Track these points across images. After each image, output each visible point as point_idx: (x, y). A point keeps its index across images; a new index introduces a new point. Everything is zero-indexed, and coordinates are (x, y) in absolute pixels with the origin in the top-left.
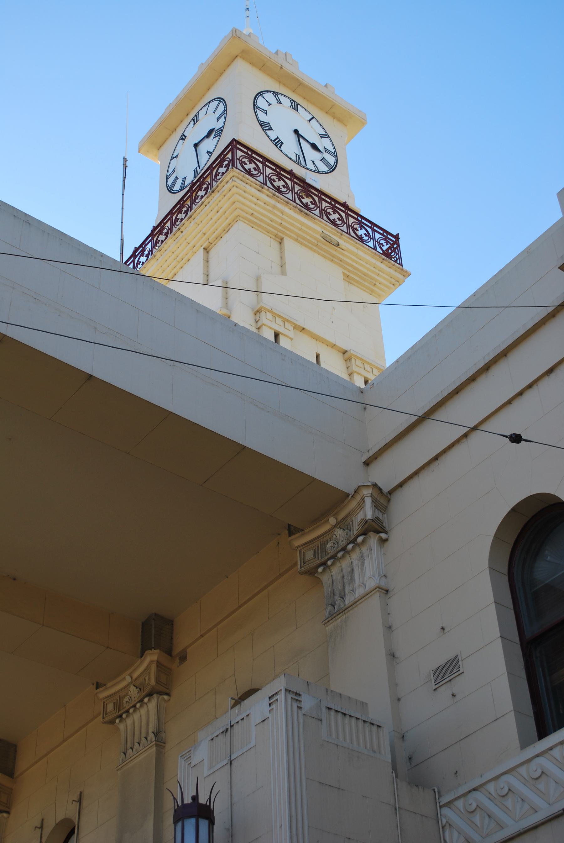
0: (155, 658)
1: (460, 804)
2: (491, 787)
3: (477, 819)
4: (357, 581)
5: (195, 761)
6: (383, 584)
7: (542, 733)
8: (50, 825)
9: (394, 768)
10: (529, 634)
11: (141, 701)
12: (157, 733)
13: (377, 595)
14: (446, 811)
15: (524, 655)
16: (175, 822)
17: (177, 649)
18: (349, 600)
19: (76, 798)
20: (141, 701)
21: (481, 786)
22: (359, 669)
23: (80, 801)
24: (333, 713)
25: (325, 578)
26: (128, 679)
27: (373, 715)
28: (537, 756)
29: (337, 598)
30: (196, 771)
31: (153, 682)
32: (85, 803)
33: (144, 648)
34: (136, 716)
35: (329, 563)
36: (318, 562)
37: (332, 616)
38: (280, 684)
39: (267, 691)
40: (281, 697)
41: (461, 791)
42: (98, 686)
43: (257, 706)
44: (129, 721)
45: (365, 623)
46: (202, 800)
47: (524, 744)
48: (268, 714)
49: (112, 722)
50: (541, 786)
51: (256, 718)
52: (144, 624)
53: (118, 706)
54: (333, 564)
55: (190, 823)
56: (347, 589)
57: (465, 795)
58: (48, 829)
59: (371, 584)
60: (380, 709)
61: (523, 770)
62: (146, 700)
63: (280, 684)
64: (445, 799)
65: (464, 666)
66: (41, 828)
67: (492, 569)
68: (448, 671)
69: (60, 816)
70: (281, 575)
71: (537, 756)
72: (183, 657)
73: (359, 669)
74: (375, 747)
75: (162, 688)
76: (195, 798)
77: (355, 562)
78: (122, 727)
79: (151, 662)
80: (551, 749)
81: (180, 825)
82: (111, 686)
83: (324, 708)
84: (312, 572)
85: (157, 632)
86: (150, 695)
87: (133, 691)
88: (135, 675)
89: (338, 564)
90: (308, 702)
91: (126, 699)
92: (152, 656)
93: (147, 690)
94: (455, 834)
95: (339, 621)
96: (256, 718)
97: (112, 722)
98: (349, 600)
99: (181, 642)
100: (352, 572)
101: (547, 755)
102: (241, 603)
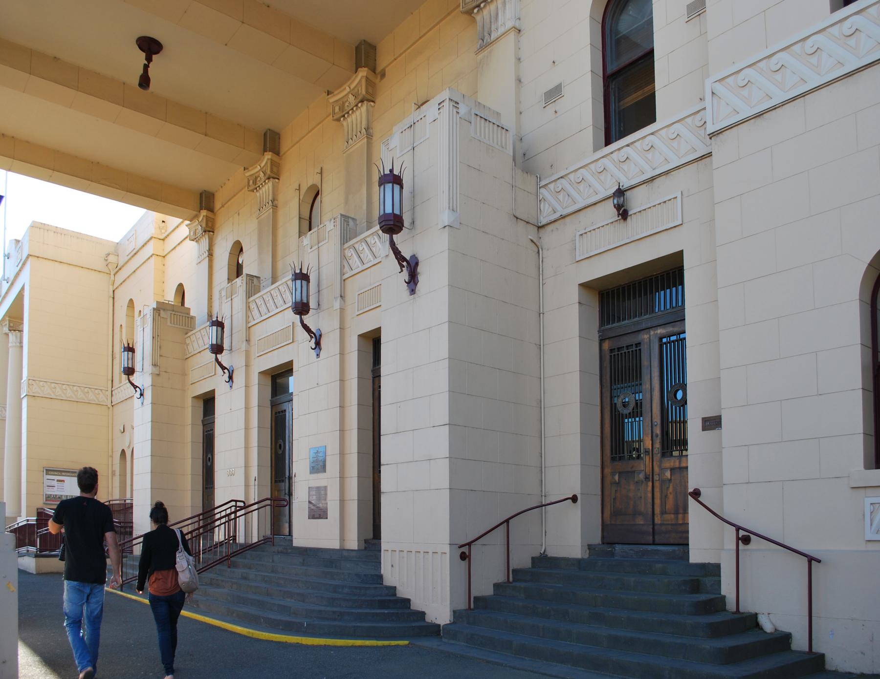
0: (365, 74)
1: (551, 186)
2: (572, 176)
3: (561, 196)
4: (500, 22)
5: (391, 146)
6: (517, 25)
7: (608, 142)
8: (304, 189)
9: (514, 160)
10: (609, 71)
11: (357, 105)
12: (367, 129)
13: (513, 33)
14: (543, 190)
15: (604, 86)
16: (380, 186)
17: (379, 69)
18: (493, 37)
19: (319, 171)
20: (357, 105)
21: (566, 175)
22: (497, 90)
23: (321, 173)
24: (478, 118)
25: (478, 18)
26: (348, 89)
27: (504, 122)
28: (603, 157)
29: (486, 34)
30: (392, 153)
31: (364, 92)
32: (324, 175)
33: (358, 66)
34: (354, 116)
35: (482, 5)
36: (474, 4)
37: (482, 48)
38: (445, 95)
39: (438, 99)
40: (446, 104)
41: (553, 178)
42: (329, 93)
43: (430, 110)
44: (349, 120)
45: (504, 51)
46: (396, 172)
47: (596, 149)
48: (437, 116)
49: (338, 120)
50: (602, 177)
51: (429, 119)
52: (357, 48)
53: (342, 108)
54: (485, 6)
55: (389, 186)
56: (493, 28)
57: (555, 181)
58: (303, 191)
59: (509, 25)
60: (507, 120)
61: (592, 166)
62: (360, 105)
63: (445, 95)
64: (543, 183)
65: (565, 91)
66: (299, 190)
67: (592, 18)
68: (554, 94)
69: (310, 183)
70: (449, 14)
71: (603, 157)
72: (383, 75)
73: (497, 90)
74: (196, 519)
75: (369, 98)
76: (391, 171)
77: (500, 6)
78: (345, 123)
79: (362, 77)
80: (612, 153)
81: (382, 187)
82: (337, 94)
83: (473, 115)
84: (469, 12)
85: (365, 55)
86: (362, 101)
87: (351, 98)
88: (352, 86)
89: (488, 7)
90: (463, 109)
91: (347, 104)
92: (363, 72)
93: (360, 98)
94: (547, 205)
95: (486, 52)
96: (429, 119)
97: (338, 120)
98: (493, 37)
99: (382, 63)
100: (497, 14)
101: (863, 13)
102: (422, 34)
